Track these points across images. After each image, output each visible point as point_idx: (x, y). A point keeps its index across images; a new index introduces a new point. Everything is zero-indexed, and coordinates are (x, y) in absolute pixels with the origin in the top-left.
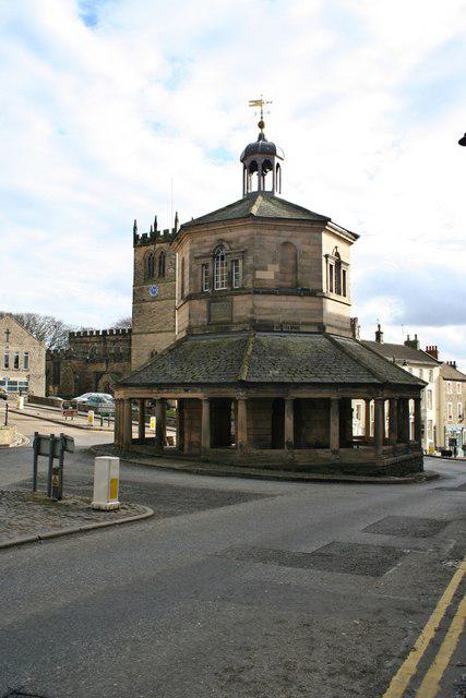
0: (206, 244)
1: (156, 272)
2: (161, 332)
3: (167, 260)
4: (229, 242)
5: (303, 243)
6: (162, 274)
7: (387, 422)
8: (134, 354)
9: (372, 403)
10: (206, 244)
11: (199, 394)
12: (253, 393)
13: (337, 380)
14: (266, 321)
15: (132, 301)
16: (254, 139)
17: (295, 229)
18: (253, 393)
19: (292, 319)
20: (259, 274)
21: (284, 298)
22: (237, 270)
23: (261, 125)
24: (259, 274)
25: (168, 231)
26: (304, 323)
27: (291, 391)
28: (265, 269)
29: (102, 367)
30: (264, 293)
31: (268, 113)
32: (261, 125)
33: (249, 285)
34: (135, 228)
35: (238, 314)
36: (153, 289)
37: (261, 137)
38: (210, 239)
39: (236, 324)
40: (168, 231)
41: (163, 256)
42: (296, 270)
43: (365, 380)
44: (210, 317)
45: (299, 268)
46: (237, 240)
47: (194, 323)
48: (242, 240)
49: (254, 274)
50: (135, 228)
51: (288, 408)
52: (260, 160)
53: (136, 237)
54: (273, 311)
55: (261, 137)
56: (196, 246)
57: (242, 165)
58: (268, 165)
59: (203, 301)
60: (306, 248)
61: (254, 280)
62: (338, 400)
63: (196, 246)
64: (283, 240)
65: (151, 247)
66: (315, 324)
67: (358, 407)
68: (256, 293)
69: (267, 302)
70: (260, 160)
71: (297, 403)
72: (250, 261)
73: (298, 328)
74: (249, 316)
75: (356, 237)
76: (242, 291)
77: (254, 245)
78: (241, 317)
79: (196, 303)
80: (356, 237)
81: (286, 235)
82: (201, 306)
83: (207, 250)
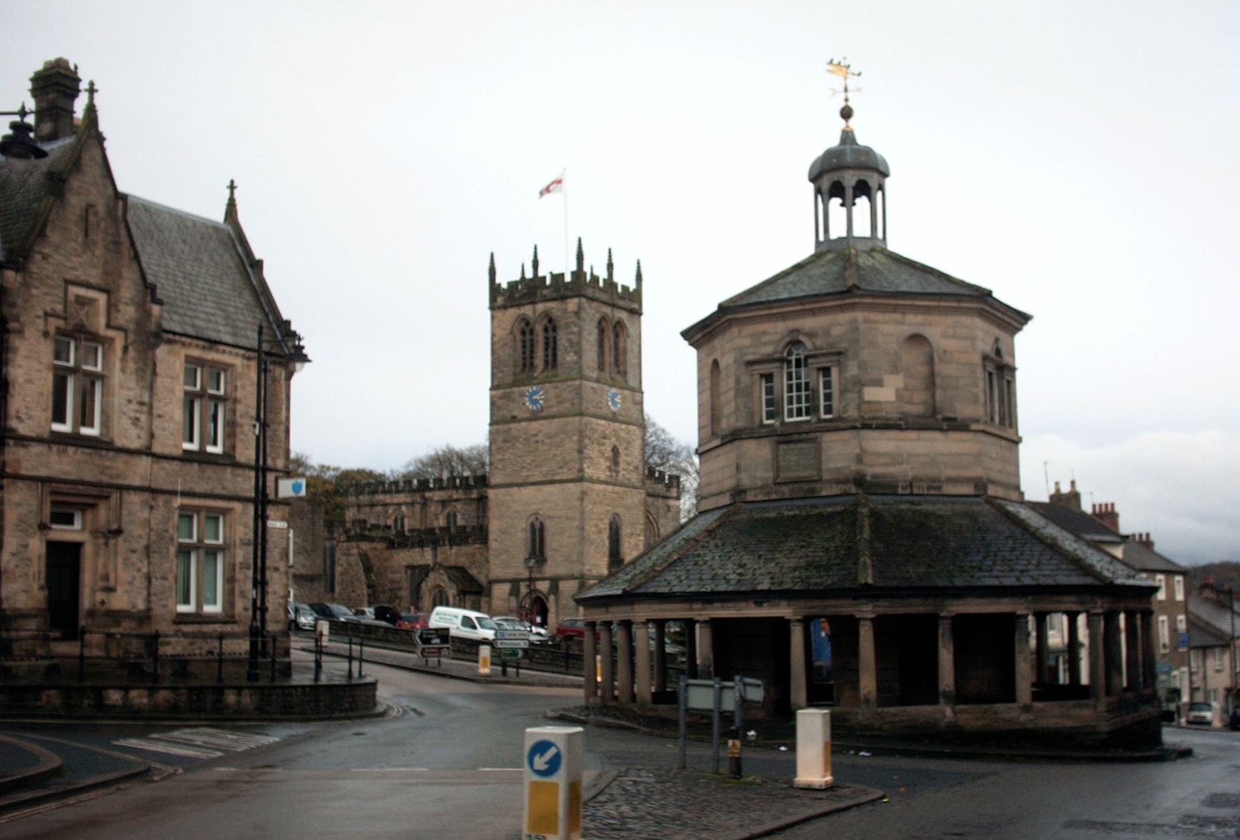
0: (766, 338)
1: (539, 361)
2: (552, 482)
3: (563, 340)
4: (812, 335)
5: (944, 336)
6: (552, 361)
7: (29, 721)
8: (494, 526)
9: (1082, 620)
10: (766, 338)
11: (783, 610)
12: (885, 607)
13: (1027, 581)
14: (884, 476)
15: (487, 419)
16: (833, 141)
17: (928, 310)
18: (885, 607)
19: (933, 472)
20: (870, 394)
21: (912, 435)
22: (827, 385)
23: (846, 113)
24: (870, 394)
25: (562, 275)
26: (950, 480)
27: (948, 602)
28: (878, 383)
29: (425, 556)
30: (880, 427)
31: (859, 90)
32: (846, 113)
33: (852, 413)
34: (492, 272)
35: (832, 465)
36: (536, 395)
37: (847, 137)
38: (774, 332)
39: (831, 482)
40: (562, 275)
41: (551, 325)
42: (931, 382)
43: (1063, 580)
44: (777, 469)
45: (938, 381)
46: (827, 332)
47: (746, 481)
48: (836, 331)
49: (860, 393)
50: (492, 272)
51: (944, 631)
52: (850, 179)
53: (494, 289)
54: (896, 459)
55: (847, 137)
56: (747, 341)
57: (811, 187)
58: (863, 189)
59: (764, 442)
60: (950, 344)
61: (861, 402)
62: (872, 620)
63: (747, 341)
64: (909, 330)
65: (527, 310)
66: (968, 480)
67: (501, 644)
68: (866, 426)
69: (883, 443)
70: (850, 179)
71: (960, 621)
72: (853, 370)
73: (940, 488)
74: (854, 467)
75: (1024, 318)
76: (839, 425)
77: (857, 340)
78: (838, 470)
79: (750, 446)
80: (1024, 318)
81: (913, 322)
82: (758, 453)
83: (768, 350)
